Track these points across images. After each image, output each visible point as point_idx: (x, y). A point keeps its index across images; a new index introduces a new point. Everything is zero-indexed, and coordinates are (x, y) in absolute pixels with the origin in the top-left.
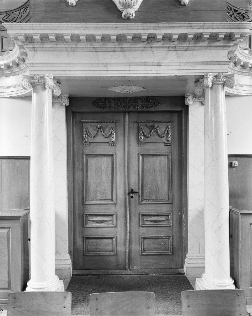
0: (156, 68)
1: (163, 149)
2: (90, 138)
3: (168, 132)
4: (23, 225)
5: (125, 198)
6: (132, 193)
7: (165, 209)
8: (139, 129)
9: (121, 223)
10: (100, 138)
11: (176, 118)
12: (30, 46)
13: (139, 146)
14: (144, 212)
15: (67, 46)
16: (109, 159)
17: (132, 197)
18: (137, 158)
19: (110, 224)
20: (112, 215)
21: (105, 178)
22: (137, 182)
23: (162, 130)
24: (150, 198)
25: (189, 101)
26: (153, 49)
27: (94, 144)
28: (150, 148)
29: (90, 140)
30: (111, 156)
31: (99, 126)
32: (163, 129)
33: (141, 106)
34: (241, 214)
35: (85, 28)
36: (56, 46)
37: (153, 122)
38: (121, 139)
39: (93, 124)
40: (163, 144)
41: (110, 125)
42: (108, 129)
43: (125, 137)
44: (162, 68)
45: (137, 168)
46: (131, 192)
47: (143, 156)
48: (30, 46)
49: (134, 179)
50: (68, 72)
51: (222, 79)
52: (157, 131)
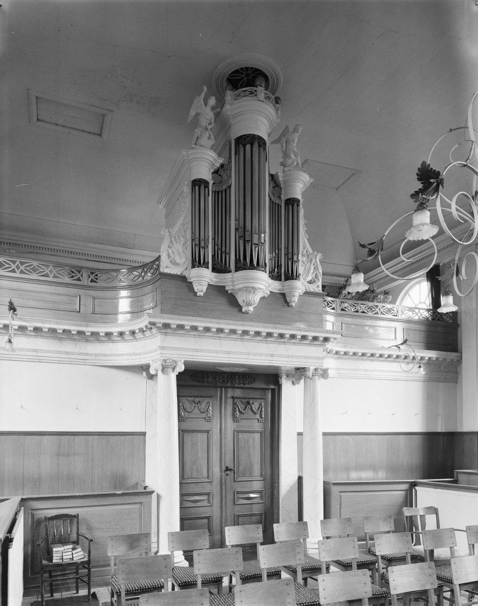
2: (186, 413)
3: (262, 409)
5: (221, 476)
6: (227, 470)
9: (216, 501)
12: (164, 331)
13: (234, 422)
15: (196, 334)
16: (205, 435)
17: (227, 475)
19: (206, 503)
20: (208, 494)
21: (202, 455)
23: (255, 406)
24: (244, 475)
26: (267, 342)
27: (190, 419)
28: (245, 424)
30: (208, 432)
31: (197, 400)
33: (238, 382)
35: (217, 323)
36: (186, 333)
37: (249, 398)
39: (189, 399)
40: (256, 421)
41: (207, 400)
43: (221, 413)
45: (232, 444)
46: (227, 469)
47: (238, 432)
48: (164, 331)
50: (195, 357)
51: (320, 372)
52: (252, 407)
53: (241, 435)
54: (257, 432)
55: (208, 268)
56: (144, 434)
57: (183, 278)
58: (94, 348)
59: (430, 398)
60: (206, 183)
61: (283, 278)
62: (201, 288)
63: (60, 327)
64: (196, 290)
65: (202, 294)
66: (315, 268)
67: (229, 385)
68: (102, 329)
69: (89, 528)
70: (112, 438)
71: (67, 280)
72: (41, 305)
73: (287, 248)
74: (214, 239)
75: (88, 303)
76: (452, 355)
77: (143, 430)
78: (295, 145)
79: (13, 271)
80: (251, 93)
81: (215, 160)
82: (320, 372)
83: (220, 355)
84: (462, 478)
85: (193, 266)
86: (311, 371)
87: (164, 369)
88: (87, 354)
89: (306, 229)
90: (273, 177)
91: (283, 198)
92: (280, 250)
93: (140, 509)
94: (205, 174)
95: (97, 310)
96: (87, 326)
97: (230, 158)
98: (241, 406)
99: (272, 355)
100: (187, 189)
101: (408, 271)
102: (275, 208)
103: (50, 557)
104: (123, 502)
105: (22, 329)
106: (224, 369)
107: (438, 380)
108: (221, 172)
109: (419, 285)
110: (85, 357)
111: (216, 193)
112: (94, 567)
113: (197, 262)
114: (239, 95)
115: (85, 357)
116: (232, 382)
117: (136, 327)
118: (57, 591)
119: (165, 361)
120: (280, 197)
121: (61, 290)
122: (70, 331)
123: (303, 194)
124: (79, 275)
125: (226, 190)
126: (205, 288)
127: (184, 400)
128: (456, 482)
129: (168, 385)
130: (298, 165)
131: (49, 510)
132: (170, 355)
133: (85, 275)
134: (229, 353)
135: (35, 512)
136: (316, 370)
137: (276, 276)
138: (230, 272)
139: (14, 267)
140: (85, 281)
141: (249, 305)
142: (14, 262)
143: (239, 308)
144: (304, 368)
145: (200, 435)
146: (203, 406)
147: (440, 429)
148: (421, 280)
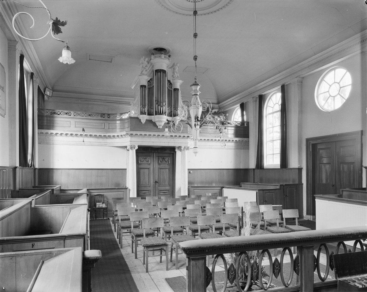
0: (168, 144)
1: (167, 166)
4: (7, 223)
7: (168, 188)
8: (159, 159)
10: (145, 162)
11: (171, 155)
14: (160, 189)
17: (156, 184)
18: (158, 169)
20: (149, 191)
22: (33, 177)
25: (177, 150)
28: (162, 166)
29: (141, 162)
30: (149, 169)
31: (145, 157)
32: (167, 159)
34: (191, 187)
38: (152, 162)
42: (147, 159)
44: (169, 144)
46: (156, 182)
47: (160, 169)
49: (157, 176)
51: (186, 148)
53: (161, 170)
54: (167, 169)
55: (146, 114)
56: (126, 169)
57: (137, 118)
58: (109, 141)
59: (237, 156)
60: (145, 86)
61: (173, 116)
62: (143, 121)
63: (98, 134)
64: (142, 122)
65: (144, 123)
66: (185, 111)
67: (156, 152)
68: (112, 134)
69: (107, 199)
70: (115, 171)
71: (100, 118)
72: (92, 127)
73: (174, 106)
74: (148, 104)
75: (107, 125)
76: (246, 139)
77: (126, 168)
78: (177, 70)
79: (83, 116)
80: (160, 56)
81: (148, 78)
82: (186, 148)
83: (150, 143)
84: (242, 185)
85: (141, 114)
86: (183, 148)
87: (131, 148)
88: (107, 143)
89: (181, 98)
90: (169, 81)
91: (173, 88)
92: (172, 106)
93: (123, 194)
94: (145, 83)
95: (110, 127)
96: (107, 134)
97: (153, 77)
98: (161, 160)
99: (169, 143)
100: (139, 88)
101: (234, 103)
102: (170, 92)
103: (95, 205)
104: (118, 191)
105: (86, 135)
106: (154, 147)
107: (237, 149)
108: (150, 81)
109: (334, 71)
110: (106, 144)
111: (149, 89)
112: (108, 211)
113: (142, 113)
114: (155, 57)
115: (106, 144)
116: (157, 151)
117: (122, 134)
118: (98, 218)
119: (131, 146)
120: (172, 88)
121: (98, 121)
122: (101, 135)
123: (181, 86)
124: (104, 116)
125: (152, 87)
126: (145, 121)
127: (141, 158)
128: (241, 187)
129: (132, 154)
130: (178, 77)
131: (95, 193)
132: (133, 144)
133: (106, 116)
134: (154, 142)
135: (91, 193)
136: (185, 147)
137: (170, 115)
138: (153, 115)
139: (83, 115)
140: (106, 118)
141: (160, 126)
142: (83, 113)
143: (157, 127)
144: (181, 147)
145: (146, 170)
146: (147, 159)
147: (241, 168)
148: (337, 67)
